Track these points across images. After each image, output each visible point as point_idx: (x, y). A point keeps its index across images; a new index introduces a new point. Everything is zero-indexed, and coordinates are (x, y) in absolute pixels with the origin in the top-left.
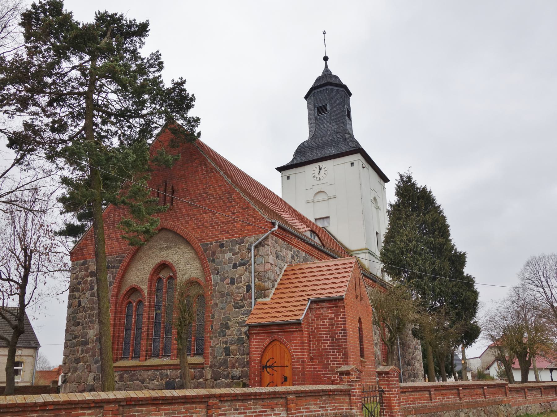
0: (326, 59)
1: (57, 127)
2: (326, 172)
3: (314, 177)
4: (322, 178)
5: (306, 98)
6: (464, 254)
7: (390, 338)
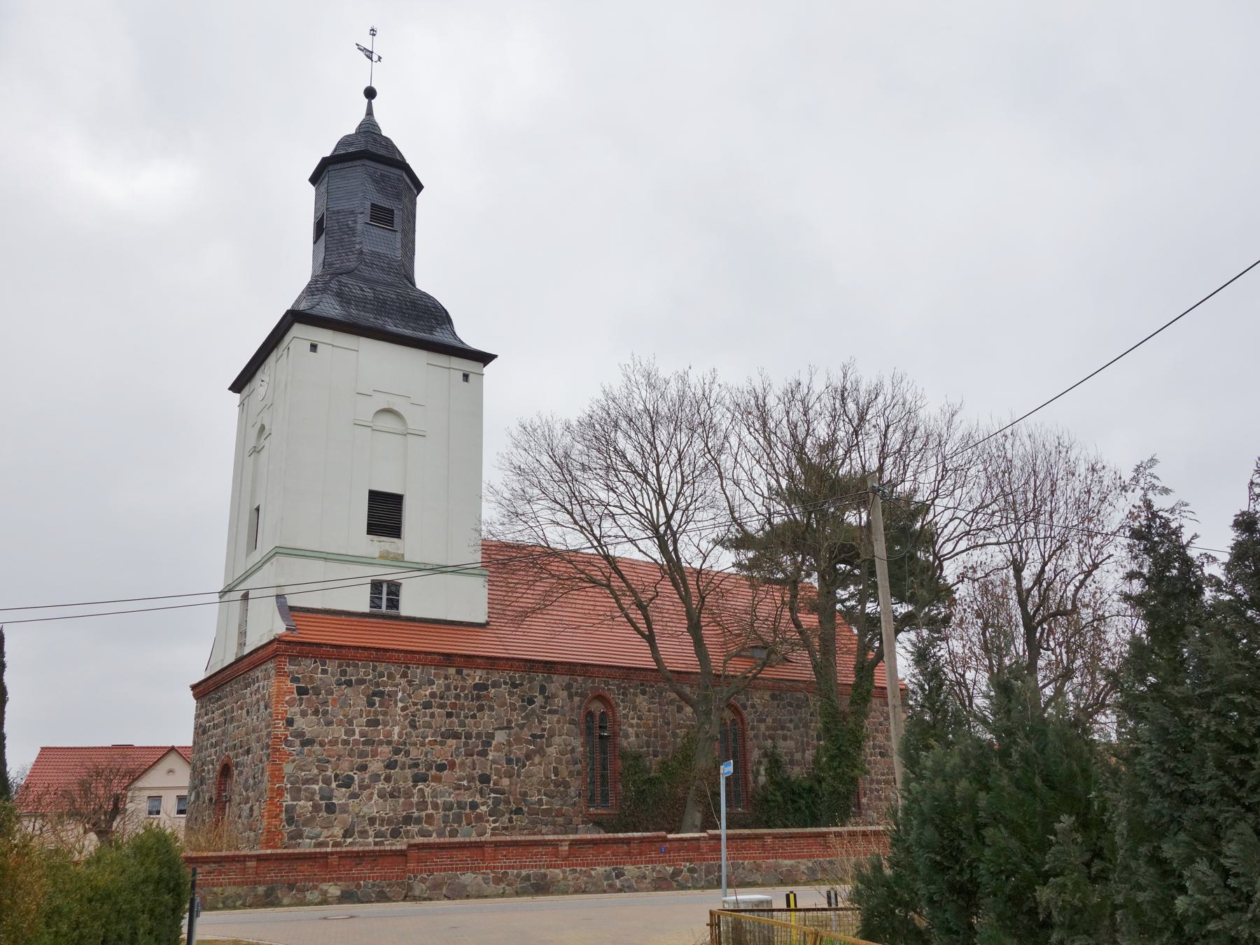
0: (370, 93)
5: (314, 179)
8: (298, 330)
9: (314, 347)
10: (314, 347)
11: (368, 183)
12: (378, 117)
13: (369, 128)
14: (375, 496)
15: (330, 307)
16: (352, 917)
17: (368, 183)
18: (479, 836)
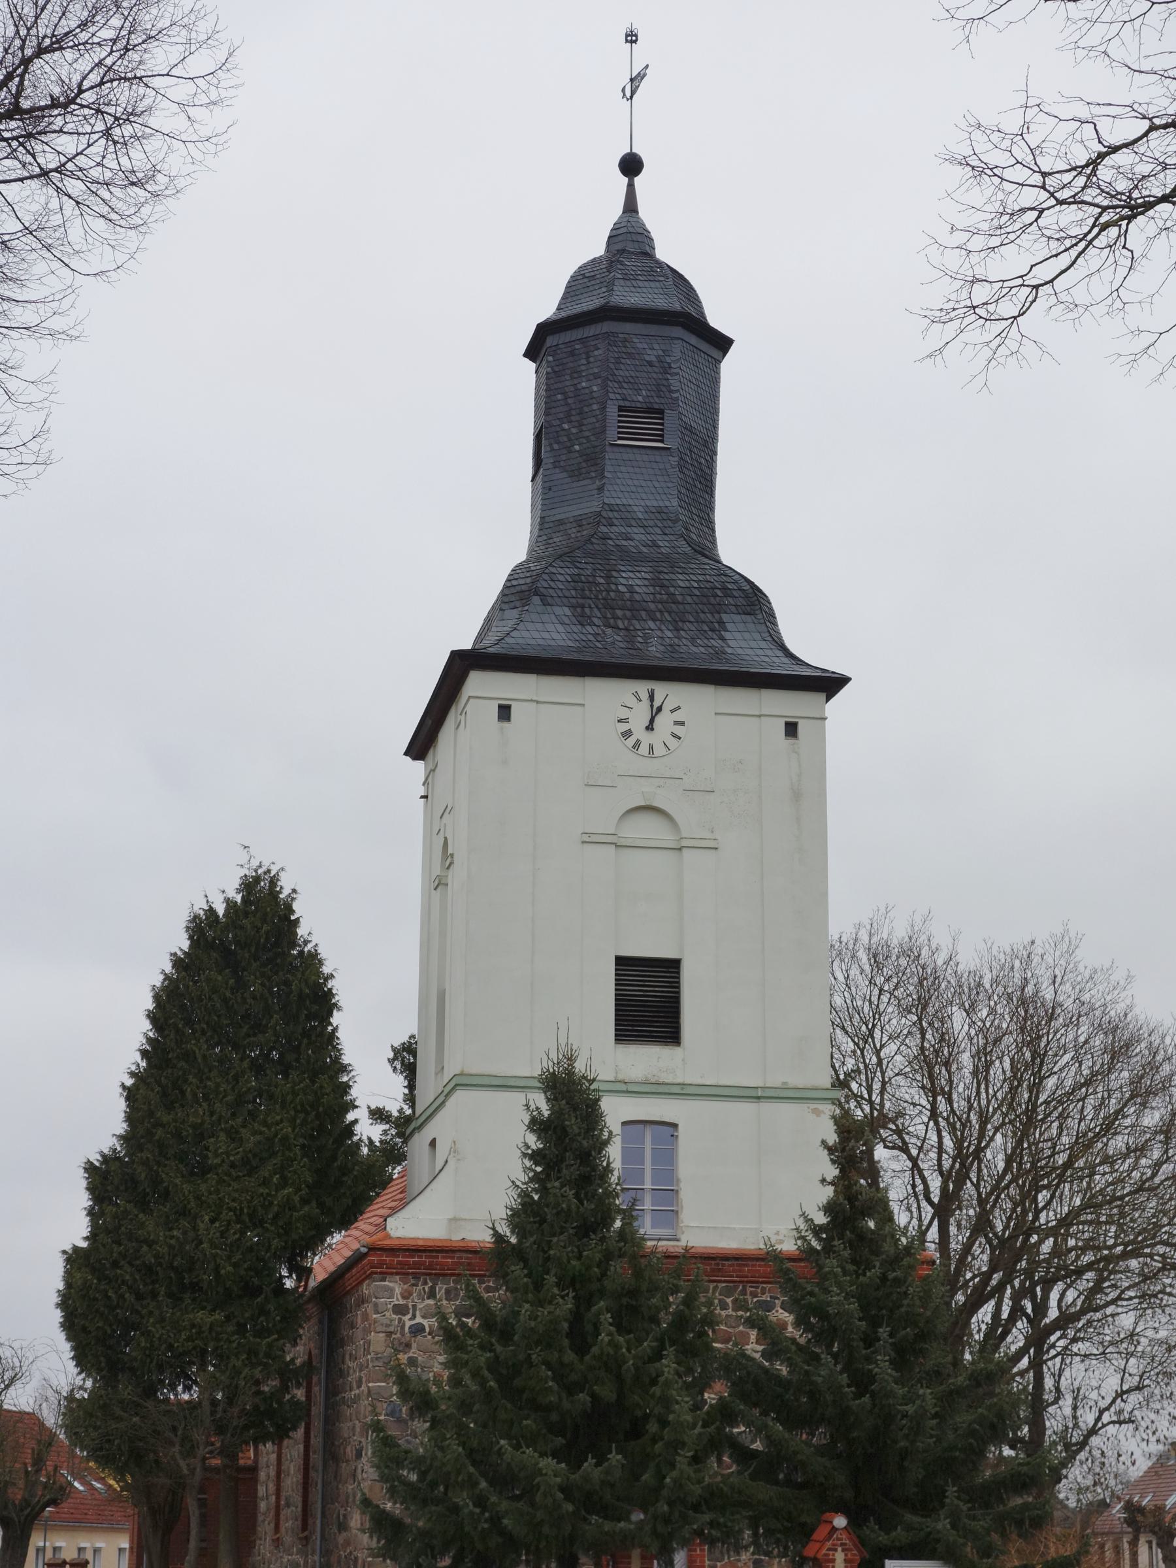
0: (631, 166)
1: (876, 1224)
2: (678, 730)
3: (627, 734)
4: (659, 750)
5: (532, 353)
6: (406, 754)
7: (1014, 1325)
8: (482, 686)
9: (505, 712)
10: (505, 712)
11: (626, 363)
12: (646, 213)
13: (630, 242)
14: (628, 967)
15: (550, 632)
16: (797, 795)
17: (626, 363)
18: (762, 1560)
